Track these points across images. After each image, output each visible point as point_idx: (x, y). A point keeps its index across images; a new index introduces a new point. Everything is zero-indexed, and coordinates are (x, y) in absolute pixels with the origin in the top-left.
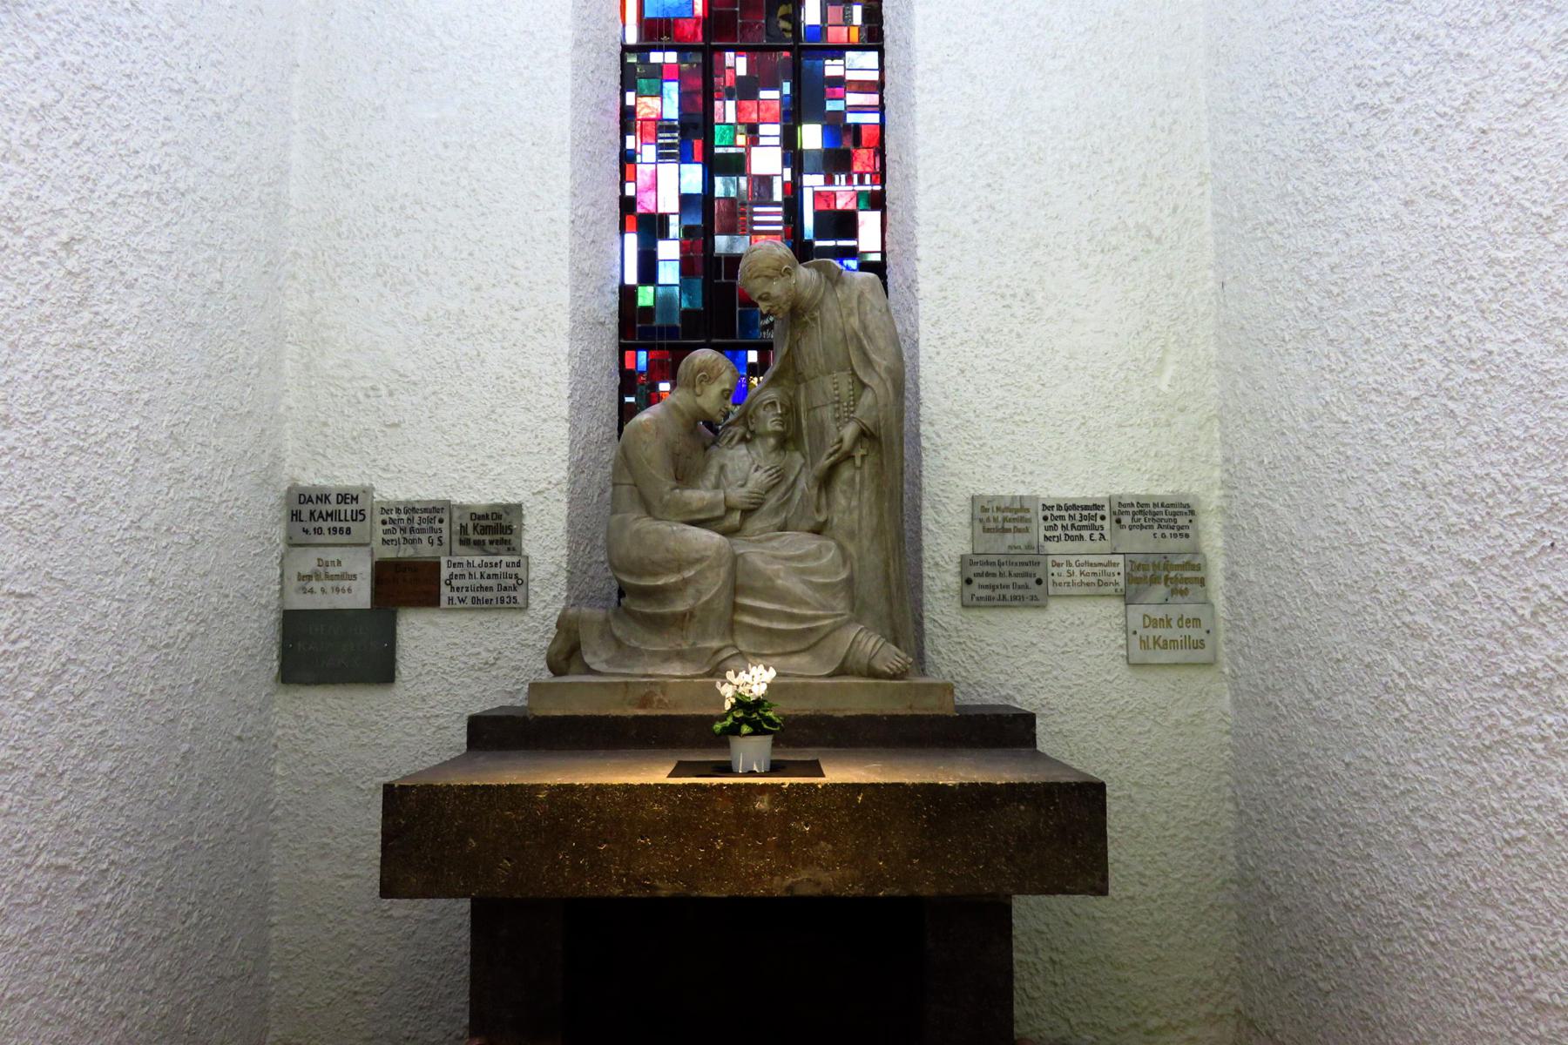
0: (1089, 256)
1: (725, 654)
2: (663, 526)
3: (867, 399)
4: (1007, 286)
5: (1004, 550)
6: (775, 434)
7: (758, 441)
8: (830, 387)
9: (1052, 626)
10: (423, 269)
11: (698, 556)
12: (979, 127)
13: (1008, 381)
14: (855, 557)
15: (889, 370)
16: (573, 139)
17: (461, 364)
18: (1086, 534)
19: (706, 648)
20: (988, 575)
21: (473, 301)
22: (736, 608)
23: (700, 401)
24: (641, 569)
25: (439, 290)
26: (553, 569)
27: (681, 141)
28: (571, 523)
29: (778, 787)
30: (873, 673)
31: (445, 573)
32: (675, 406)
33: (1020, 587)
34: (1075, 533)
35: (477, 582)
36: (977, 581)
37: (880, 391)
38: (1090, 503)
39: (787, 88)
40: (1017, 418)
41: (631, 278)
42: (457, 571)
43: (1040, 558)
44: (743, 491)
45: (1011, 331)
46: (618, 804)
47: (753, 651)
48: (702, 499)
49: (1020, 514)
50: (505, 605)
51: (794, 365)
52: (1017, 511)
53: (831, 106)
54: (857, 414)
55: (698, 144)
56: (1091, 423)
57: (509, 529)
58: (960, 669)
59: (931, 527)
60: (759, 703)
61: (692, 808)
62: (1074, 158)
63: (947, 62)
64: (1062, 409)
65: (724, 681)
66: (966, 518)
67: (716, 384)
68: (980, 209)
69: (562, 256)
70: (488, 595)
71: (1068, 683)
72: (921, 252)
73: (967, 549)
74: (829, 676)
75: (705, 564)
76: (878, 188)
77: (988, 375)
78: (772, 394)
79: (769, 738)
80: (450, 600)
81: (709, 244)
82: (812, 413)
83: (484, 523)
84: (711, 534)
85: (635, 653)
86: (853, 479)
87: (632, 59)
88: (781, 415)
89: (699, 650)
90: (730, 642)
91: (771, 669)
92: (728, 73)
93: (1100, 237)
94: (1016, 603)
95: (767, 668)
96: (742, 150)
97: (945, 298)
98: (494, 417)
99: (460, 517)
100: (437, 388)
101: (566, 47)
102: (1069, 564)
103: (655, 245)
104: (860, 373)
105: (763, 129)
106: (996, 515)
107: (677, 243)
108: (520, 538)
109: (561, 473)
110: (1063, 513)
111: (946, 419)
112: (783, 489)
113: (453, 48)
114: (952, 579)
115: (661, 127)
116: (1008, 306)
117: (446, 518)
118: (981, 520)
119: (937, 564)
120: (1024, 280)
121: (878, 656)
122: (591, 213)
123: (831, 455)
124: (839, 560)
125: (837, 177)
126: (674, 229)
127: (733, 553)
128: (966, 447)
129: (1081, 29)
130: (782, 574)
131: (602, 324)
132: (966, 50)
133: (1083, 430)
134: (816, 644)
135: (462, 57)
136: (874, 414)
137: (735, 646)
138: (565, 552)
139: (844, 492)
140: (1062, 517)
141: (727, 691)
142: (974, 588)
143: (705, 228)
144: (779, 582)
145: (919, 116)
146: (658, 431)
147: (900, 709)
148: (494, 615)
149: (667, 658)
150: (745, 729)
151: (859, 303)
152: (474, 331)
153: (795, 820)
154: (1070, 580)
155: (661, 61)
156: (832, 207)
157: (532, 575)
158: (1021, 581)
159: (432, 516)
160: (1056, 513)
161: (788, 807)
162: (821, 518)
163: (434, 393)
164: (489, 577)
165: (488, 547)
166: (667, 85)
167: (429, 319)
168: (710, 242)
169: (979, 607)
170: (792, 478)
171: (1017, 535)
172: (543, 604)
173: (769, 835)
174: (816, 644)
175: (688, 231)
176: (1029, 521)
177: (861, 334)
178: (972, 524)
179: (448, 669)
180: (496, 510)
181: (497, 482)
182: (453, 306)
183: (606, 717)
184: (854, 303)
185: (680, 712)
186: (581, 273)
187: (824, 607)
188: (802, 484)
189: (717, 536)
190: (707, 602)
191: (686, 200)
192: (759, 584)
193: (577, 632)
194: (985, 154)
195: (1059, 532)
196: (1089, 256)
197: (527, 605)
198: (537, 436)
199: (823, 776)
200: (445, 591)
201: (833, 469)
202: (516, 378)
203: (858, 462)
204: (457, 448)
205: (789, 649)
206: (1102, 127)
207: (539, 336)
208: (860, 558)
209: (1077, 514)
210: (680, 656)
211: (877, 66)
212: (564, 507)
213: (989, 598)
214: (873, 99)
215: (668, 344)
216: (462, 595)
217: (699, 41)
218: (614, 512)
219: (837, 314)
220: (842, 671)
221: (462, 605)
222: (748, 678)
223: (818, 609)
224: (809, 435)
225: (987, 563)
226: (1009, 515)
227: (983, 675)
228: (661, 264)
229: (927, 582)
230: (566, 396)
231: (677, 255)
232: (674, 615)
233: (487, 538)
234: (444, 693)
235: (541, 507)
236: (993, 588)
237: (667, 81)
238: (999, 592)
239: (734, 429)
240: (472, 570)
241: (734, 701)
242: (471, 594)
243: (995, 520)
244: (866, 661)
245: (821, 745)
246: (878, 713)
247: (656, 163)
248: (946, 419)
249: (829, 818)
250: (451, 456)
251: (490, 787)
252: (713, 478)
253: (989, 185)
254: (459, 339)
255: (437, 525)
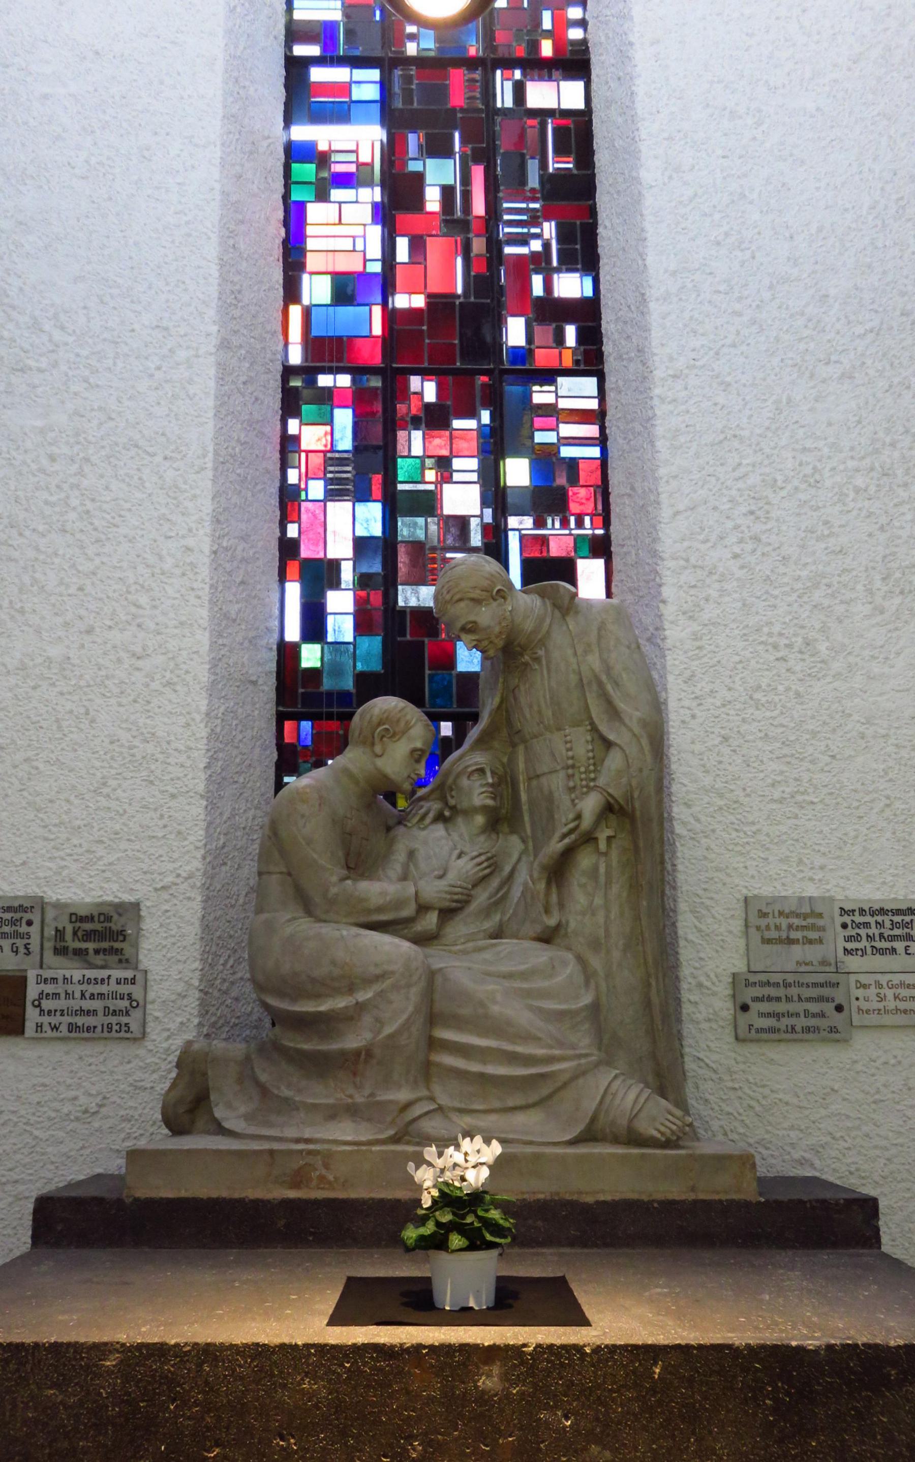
0: (884, 598)
1: (417, 1110)
2: (327, 930)
3: (614, 761)
4: (781, 634)
5: (791, 967)
6: (485, 809)
7: (460, 820)
8: (560, 748)
9: (859, 1067)
10: (18, 606)
11: (378, 971)
12: (736, 444)
13: (786, 751)
14: (601, 973)
15: (644, 724)
16: (216, 454)
17: (64, 724)
18: (899, 946)
19: (391, 1102)
20: (770, 999)
21: (83, 646)
22: (433, 1044)
23: (379, 762)
24: (298, 992)
25: (38, 632)
26: (180, 987)
27: (354, 476)
28: (206, 927)
29: (516, 1351)
30: (634, 1139)
31: (32, 991)
32: (346, 771)
33: (814, 1015)
34: (887, 945)
35: (76, 1004)
36: (755, 1007)
37: (632, 751)
38: (904, 907)
39: (485, 417)
40: (799, 798)
41: (293, 633)
42: (49, 988)
43: (840, 978)
44: (442, 884)
45: (788, 689)
46: (242, 1378)
47: (457, 1104)
48: (383, 893)
49: (810, 921)
50: (114, 1034)
51: (509, 723)
52: (805, 916)
53: (541, 437)
54: (601, 782)
55: (377, 480)
56: (898, 804)
57: (121, 935)
58: (737, 1124)
59: (691, 937)
60: (476, 1198)
61: (368, 1386)
62: (860, 481)
63: (694, 367)
64: (858, 786)
65: (420, 1161)
66: (737, 925)
67: (404, 740)
68: (741, 541)
69: (200, 593)
70: (90, 1021)
71: (884, 1143)
72: (667, 592)
73: (740, 966)
74: (572, 1143)
75: (388, 982)
76: (600, 532)
77: (760, 744)
78: (479, 759)
79: (494, 1253)
80: (39, 1027)
81: (390, 595)
82: (534, 783)
83: (88, 926)
84: (397, 940)
85: (288, 1106)
86: (596, 869)
87: (296, 383)
88: (492, 785)
89: (380, 1103)
90: (425, 1093)
91: (495, 1142)
92: (414, 401)
93: (898, 575)
94: (811, 1036)
95: (487, 1141)
96: (431, 487)
97: (700, 648)
98: (105, 791)
99: (55, 919)
100: (30, 754)
101: (209, 345)
102: (879, 985)
103: (323, 596)
104: (603, 728)
105: (457, 463)
106: (778, 921)
107: (351, 594)
108: (136, 946)
109: (195, 864)
110: (868, 919)
111: (707, 799)
112: (495, 882)
113: (66, 344)
114: (724, 1007)
115: (331, 459)
116: (783, 659)
117: (36, 918)
118: (758, 928)
119: (700, 985)
120: (803, 627)
121: (642, 1115)
122: (240, 548)
123: (564, 836)
124: (580, 979)
125: (549, 521)
126: (347, 573)
127: (429, 967)
128: (734, 834)
129: (860, 330)
130: (499, 997)
131: (254, 683)
132: (717, 354)
133: (888, 813)
134: (550, 1096)
135: (78, 355)
136: (624, 780)
137: (432, 1099)
138: (197, 965)
139: (582, 886)
140: (867, 925)
141: (425, 1177)
142: (752, 1016)
143: (385, 577)
144: (495, 1009)
145: (659, 430)
146: (322, 801)
147: (675, 1191)
148: (99, 1047)
149: (332, 1114)
150: (456, 1241)
151: (600, 637)
152: (82, 683)
153: (547, 1407)
154: (881, 1006)
155: (331, 384)
156: (545, 554)
157: (151, 995)
158: (814, 1007)
159: (17, 916)
160: (858, 919)
161: (535, 1385)
162: (552, 922)
163: (27, 760)
164: (92, 996)
165: (91, 957)
166: (338, 412)
167: (23, 667)
168: (392, 591)
169: (758, 1041)
170: (507, 869)
171: (807, 946)
172: (166, 1034)
173: (501, 1434)
174: (550, 1096)
175: (363, 581)
176: (823, 929)
177: (604, 678)
178: (746, 934)
179: (33, 1119)
180: (105, 910)
181: (108, 874)
182: (55, 652)
183: (241, 1201)
184: (593, 637)
185: (353, 1195)
186: (226, 616)
187: (561, 1044)
188: (522, 876)
189: (406, 945)
190: (391, 1036)
191: (361, 545)
192: (465, 1011)
193: (205, 1074)
194: (746, 475)
195: (864, 943)
196: (884, 598)
197: (144, 1034)
198: (162, 816)
199: (584, 1322)
200: (32, 1015)
201: (568, 854)
202: (136, 742)
203: (602, 846)
204: (54, 829)
205: (510, 1103)
206: (893, 445)
207: (167, 690)
208: (608, 976)
209: (887, 920)
210: (353, 1111)
211: (595, 394)
212: (197, 905)
213: (772, 1030)
214: (591, 430)
215: (338, 713)
216: (54, 1020)
217: (377, 360)
218: (259, 910)
219: (570, 652)
220: (589, 1136)
221: (55, 1034)
222: (458, 1158)
223: (551, 1047)
224: (532, 814)
225: (768, 983)
226: (796, 922)
227: (768, 1132)
228: (308, 254)
229: (687, 1009)
230: (202, 766)
231: (351, 609)
232: (343, 1053)
233: (91, 946)
234: (26, 1151)
235: (166, 907)
236: (777, 1016)
237: (339, 406)
238: (786, 1021)
239: (426, 805)
240: (70, 988)
241: (435, 1193)
242: (67, 1019)
243: (778, 928)
244: (625, 1122)
245: (559, 1244)
246: (645, 1198)
247: (324, 501)
248: (707, 799)
249: (605, 1405)
250: (46, 839)
251: (20, 1347)
252: (398, 868)
253: (752, 513)
254: (62, 694)
255: (24, 929)
